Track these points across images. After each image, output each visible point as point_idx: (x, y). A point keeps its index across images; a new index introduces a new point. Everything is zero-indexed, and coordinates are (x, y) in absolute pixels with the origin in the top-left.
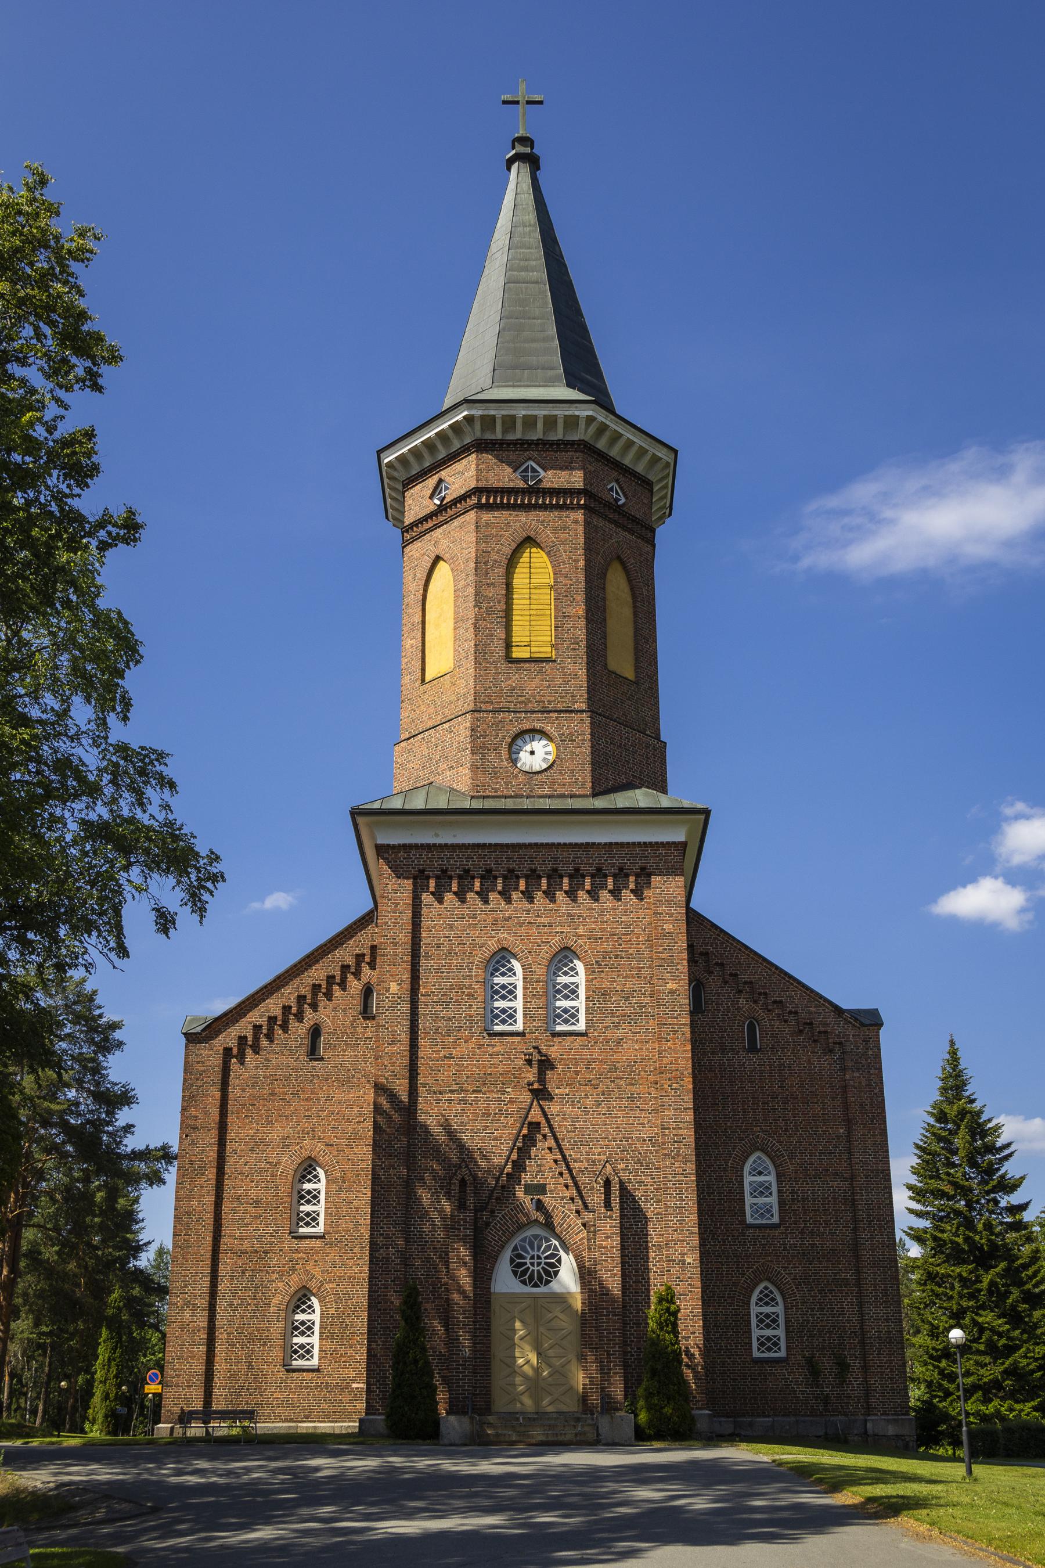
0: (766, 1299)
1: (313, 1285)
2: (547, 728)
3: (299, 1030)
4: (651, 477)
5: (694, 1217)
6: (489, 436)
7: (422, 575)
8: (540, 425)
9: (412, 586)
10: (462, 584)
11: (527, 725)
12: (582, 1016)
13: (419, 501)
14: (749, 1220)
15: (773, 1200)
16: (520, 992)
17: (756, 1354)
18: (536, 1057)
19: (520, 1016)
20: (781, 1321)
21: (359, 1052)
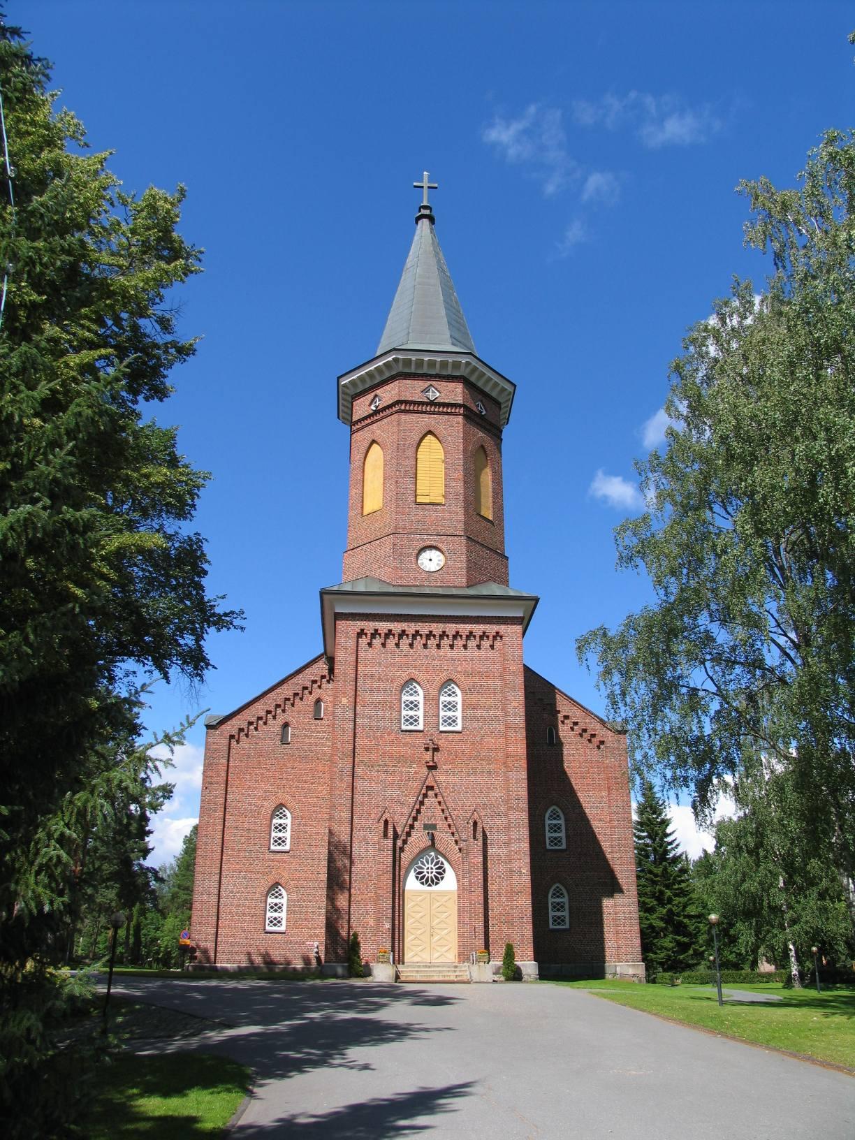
0: (558, 894)
1: (282, 881)
2: (440, 546)
3: (275, 725)
4: (501, 400)
5: (527, 845)
6: (407, 371)
7: (362, 451)
8: (438, 366)
9: (357, 456)
10: (388, 457)
11: (428, 543)
12: (459, 721)
13: (362, 407)
14: (548, 847)
15: (563, 835)
16: (421, 706)
17: (551, 927)
18: (431, 746)
19: (421, 721)
20: (567, 906)
21: (313, 740)
